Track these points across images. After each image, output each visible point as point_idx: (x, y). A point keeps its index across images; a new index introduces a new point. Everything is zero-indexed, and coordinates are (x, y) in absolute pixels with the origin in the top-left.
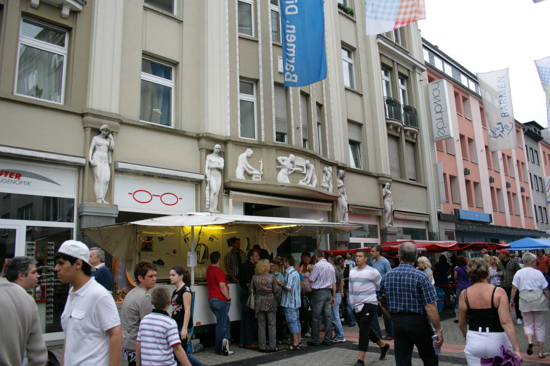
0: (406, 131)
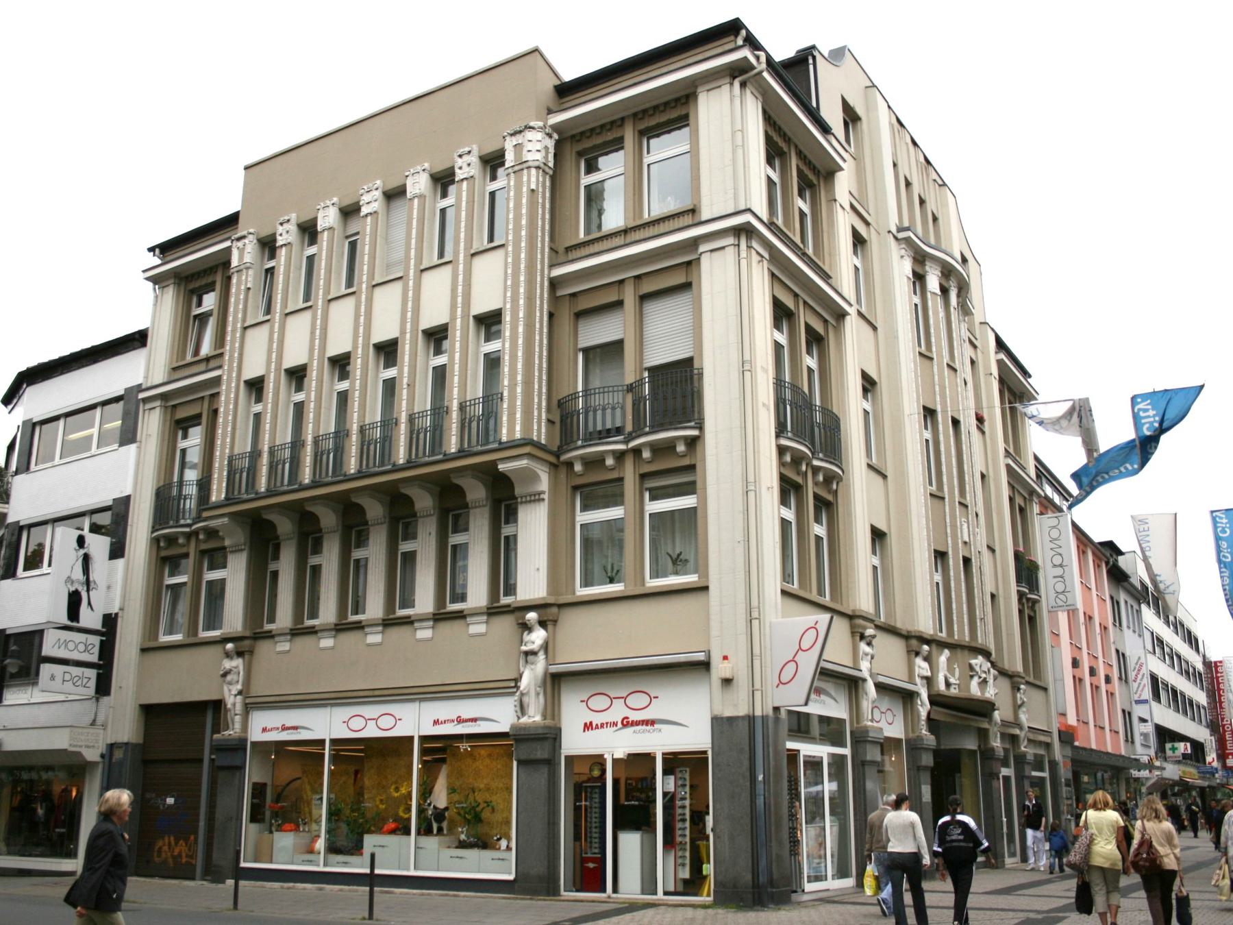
0: (816, 470)
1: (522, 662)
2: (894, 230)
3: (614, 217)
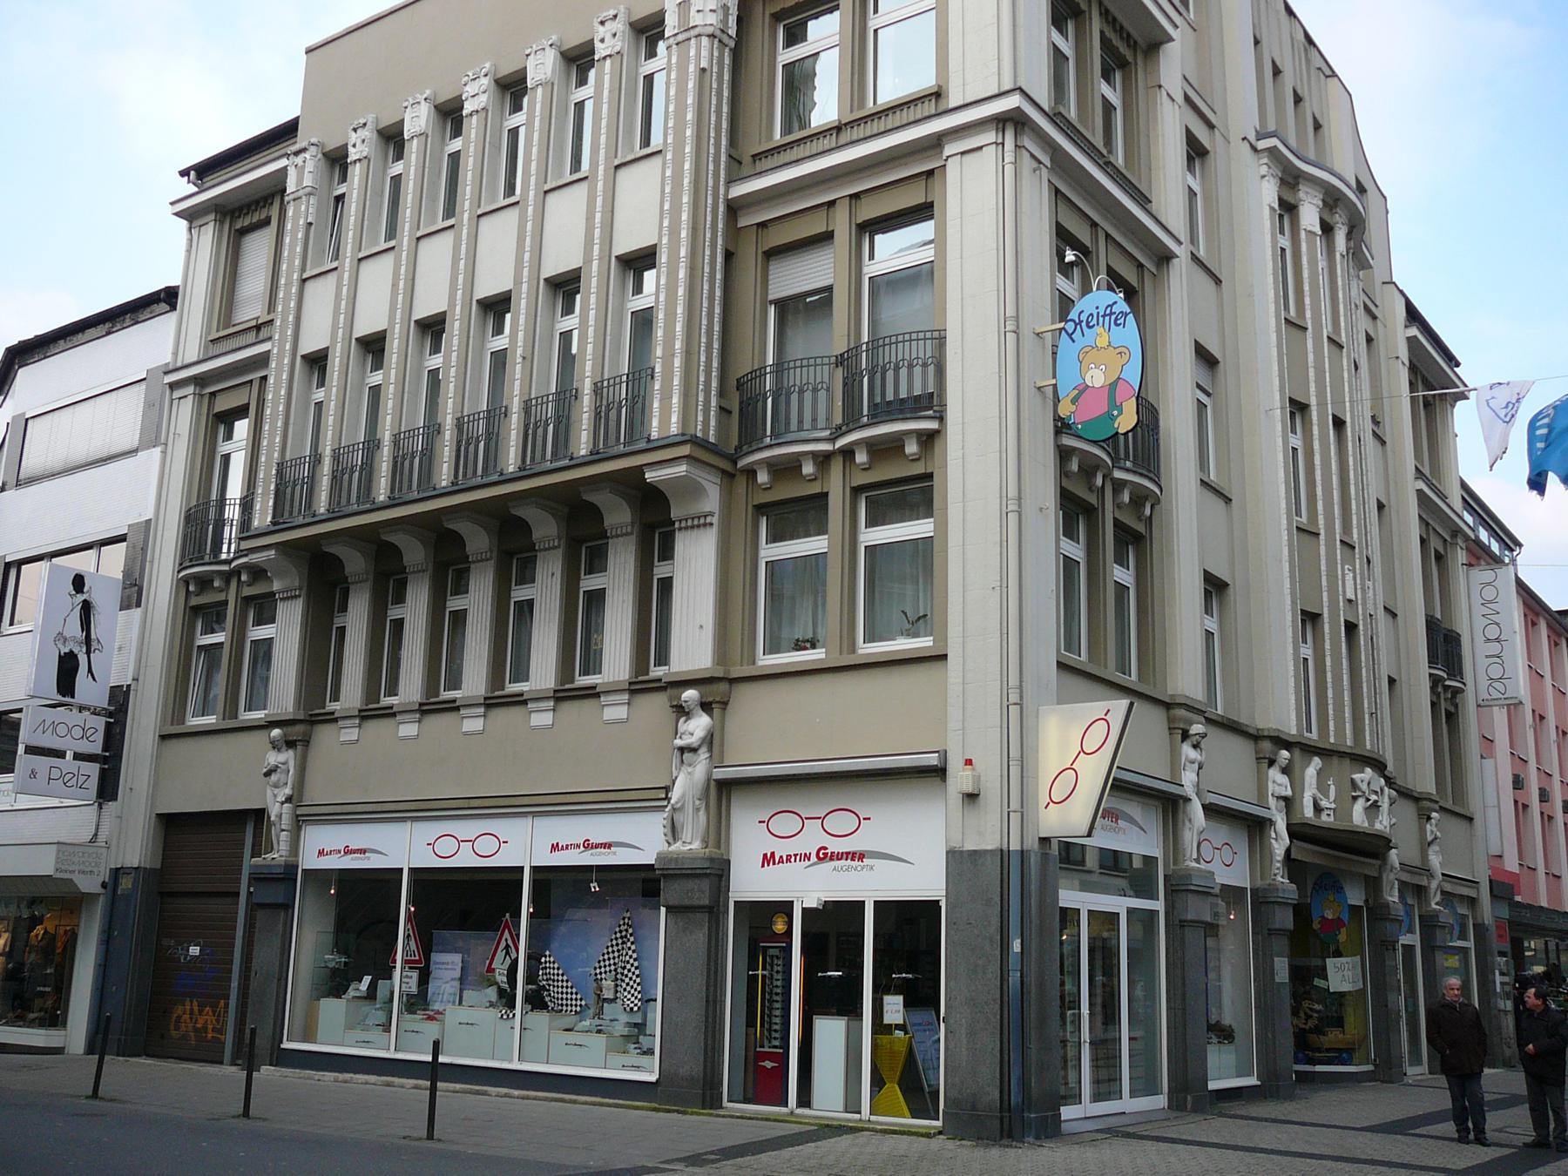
0: (1119, 486)
1: (676, 760)
2: (1252, 137)
3: (826, 108)
